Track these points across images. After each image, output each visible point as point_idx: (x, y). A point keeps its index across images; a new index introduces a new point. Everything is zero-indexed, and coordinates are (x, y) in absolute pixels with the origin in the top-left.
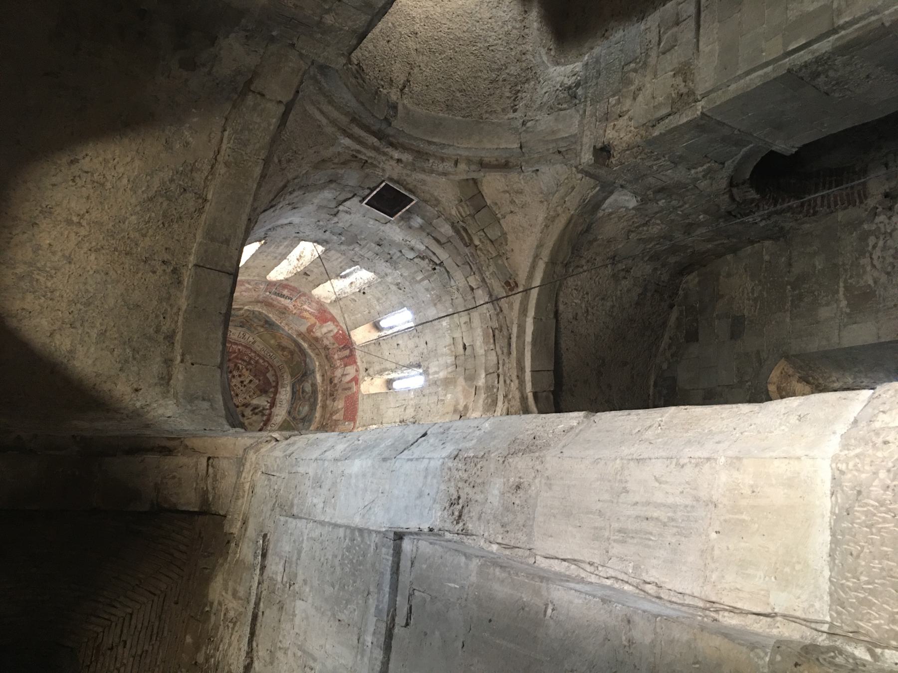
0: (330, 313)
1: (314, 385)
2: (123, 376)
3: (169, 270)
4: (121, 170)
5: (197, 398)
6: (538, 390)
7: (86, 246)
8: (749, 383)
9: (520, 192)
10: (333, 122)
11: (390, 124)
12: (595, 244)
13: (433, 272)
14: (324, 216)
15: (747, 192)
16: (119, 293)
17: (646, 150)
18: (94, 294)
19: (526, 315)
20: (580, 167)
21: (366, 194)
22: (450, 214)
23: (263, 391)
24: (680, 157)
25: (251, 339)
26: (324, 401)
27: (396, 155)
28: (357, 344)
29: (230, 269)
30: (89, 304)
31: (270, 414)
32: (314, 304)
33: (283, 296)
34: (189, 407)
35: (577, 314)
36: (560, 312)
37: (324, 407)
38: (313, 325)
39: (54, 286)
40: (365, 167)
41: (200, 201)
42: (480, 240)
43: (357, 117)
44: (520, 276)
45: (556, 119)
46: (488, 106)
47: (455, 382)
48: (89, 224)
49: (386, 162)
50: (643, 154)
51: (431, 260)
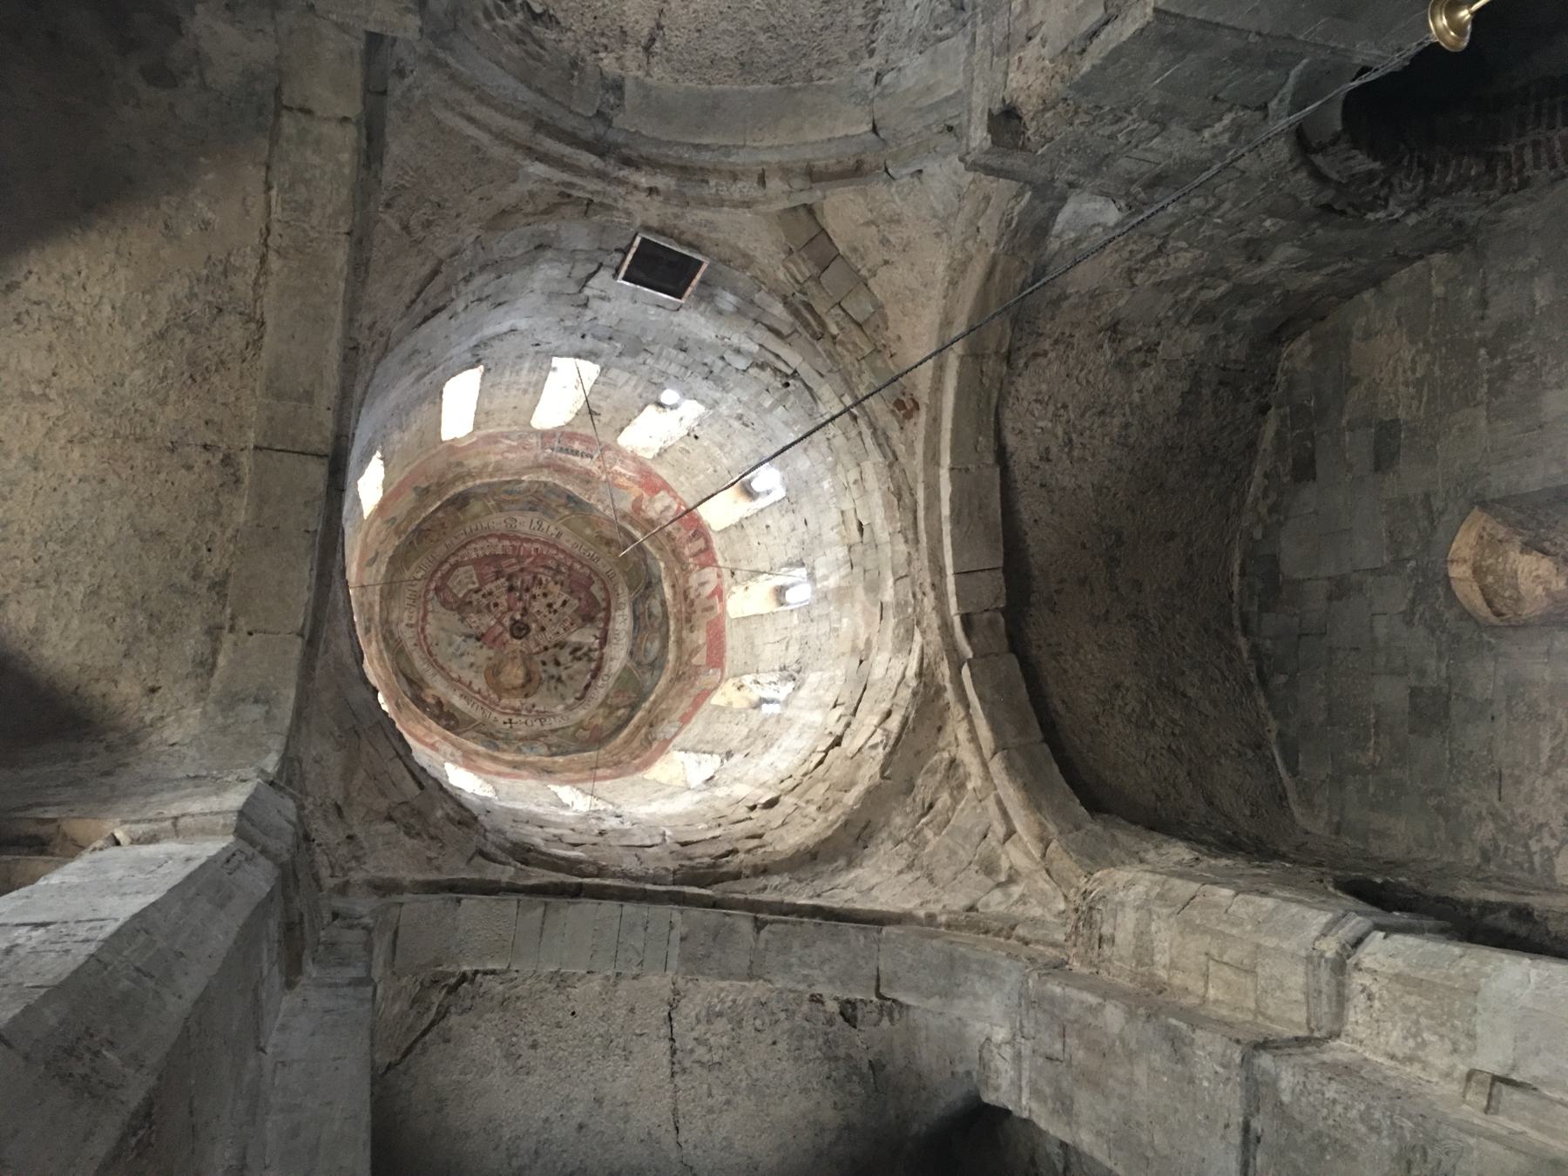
0: (659, 477)
1: (663, 603)
2: (128, 665)
3: (216, 461)
4: (97, 291)
5: (243, 700)
6: (970, 610)
7: (63, 434)
8: (1412, 564)
9: (896, 220)
10: (501, 136)
11: (608, 123)
12: (1065, 305)
13: (785, 390)
14: (566, 310)
15: (1347, 159)
16: (126, 514)
17: (1085, 106)
18: (81, 520)
19: (938, 464)
20: (969, 159)
21: (619, 260)
22: (776, 280)
23: (588, 619)
24: (1161, 108)
25: (552, 529)
26: (679, 631)
27: (643, 180)
28: (713, 527)
29: (323, 447)
30: (70, 542)
31: (601, 658)
32: (628, 462)
33: (576, 453)
34: (220, 720)
35: (1047, 449)
36: (1010, 449)
37: (680, 642)
38: (639, 499)
39: (8, 515)
40: (590, 212)
41: (253, 326)
42: (837, 324)
43: (545, 118)
44: (920, 387)
45: (933, 62)
46: (822, 51)
47: (853, 595)
48: (61, 395)
49: (629, 197)
50: (1082, 115)
51: (776, 370)
